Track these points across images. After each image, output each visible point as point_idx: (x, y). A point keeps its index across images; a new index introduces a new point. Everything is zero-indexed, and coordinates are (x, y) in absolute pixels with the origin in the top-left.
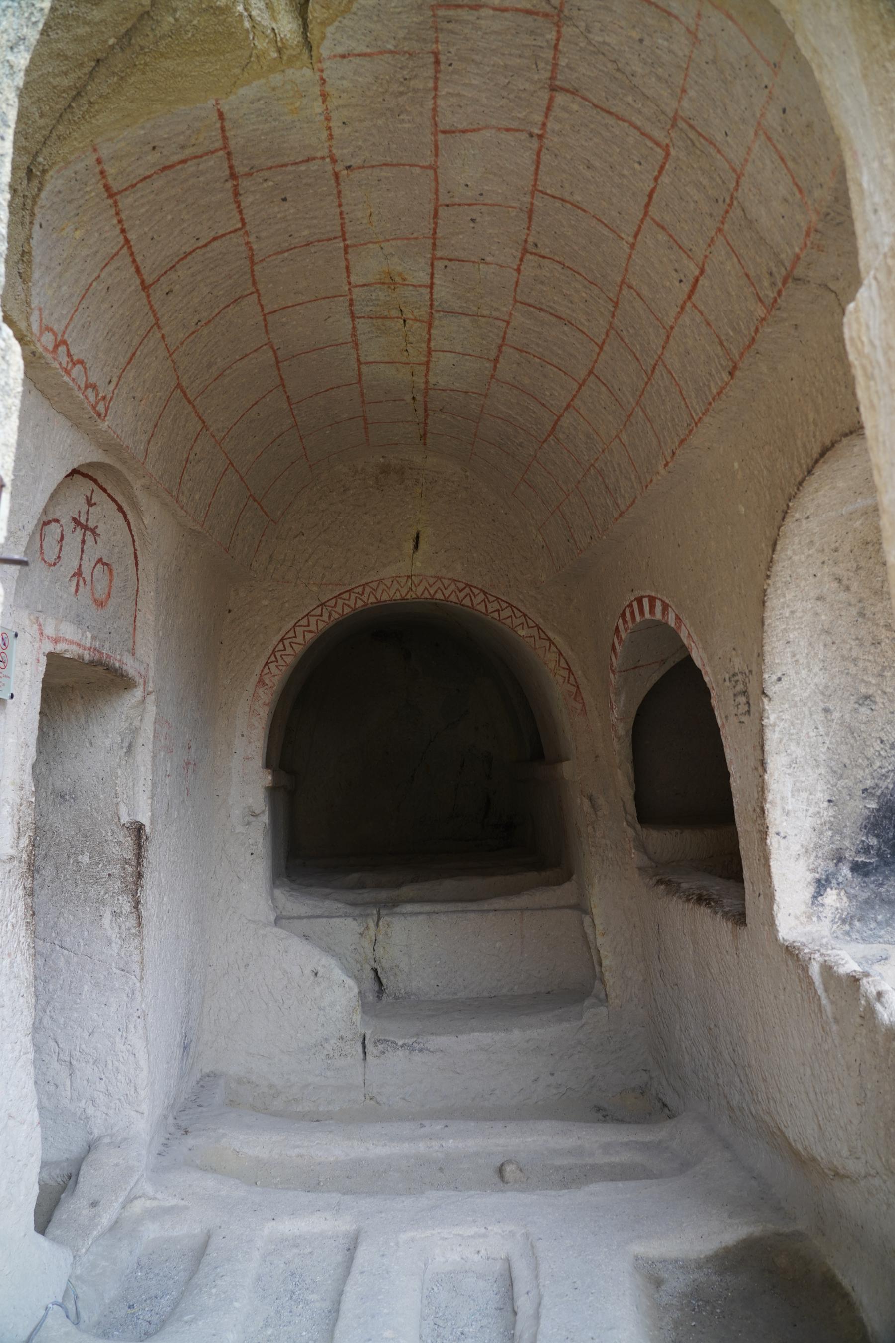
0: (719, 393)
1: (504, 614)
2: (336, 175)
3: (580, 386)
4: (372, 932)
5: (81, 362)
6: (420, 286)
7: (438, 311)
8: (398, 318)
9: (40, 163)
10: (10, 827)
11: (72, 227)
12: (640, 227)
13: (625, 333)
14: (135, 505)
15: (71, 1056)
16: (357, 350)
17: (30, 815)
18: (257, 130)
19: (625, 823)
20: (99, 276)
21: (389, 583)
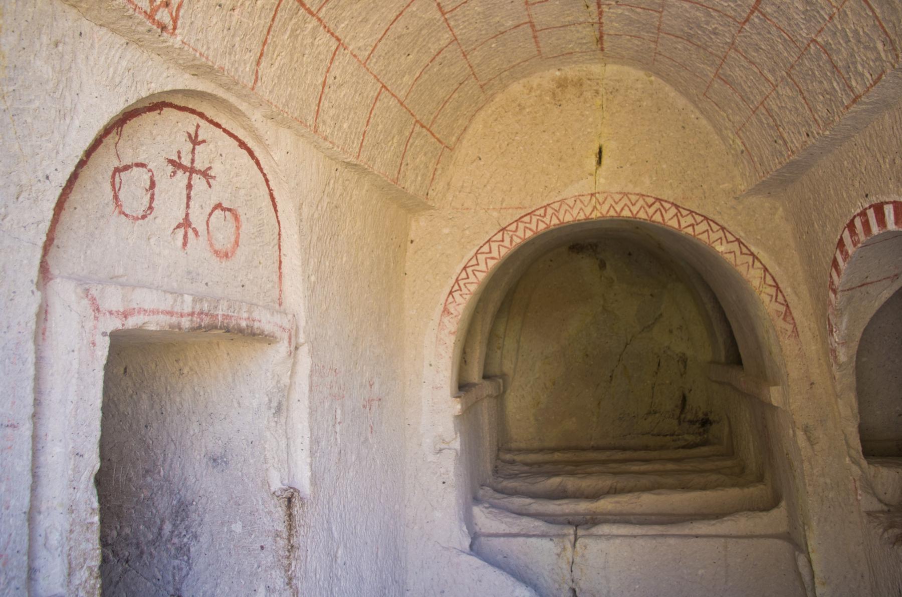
10: (58, 560)
14: (259, 139)
19: (847, 459)
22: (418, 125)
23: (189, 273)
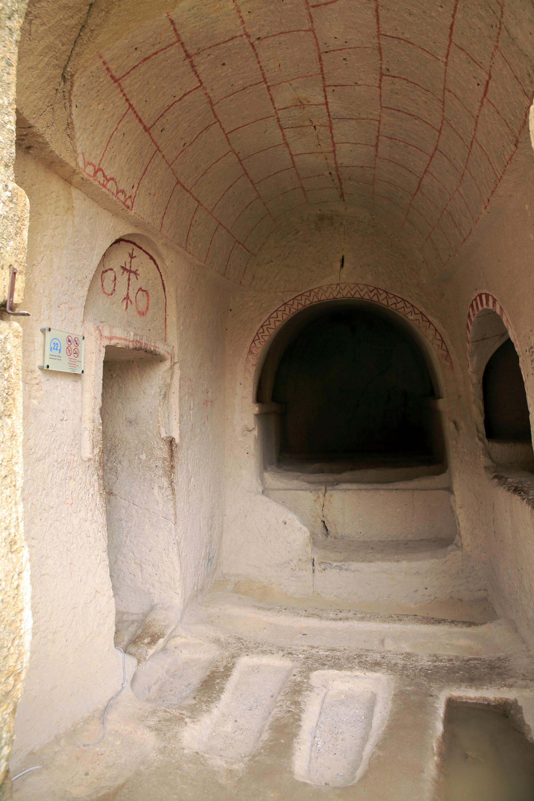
0: (510, 159)
1: (399, 306)
2: (252, 45)
3: (431, 158)
4: (321, 500)
5: (112, 179)
6: (319, 104)
7: (334, 119)
8: (310, 126)
9: (69, 72)
10: (88, 443)
11: (96, 103)
12: (448, 50)
13: (452, 122)
14: (159, 255)
15: (141, 561)
16: (289, 148)
17: (99, 436)
18: (196, 26)
19: (477, 438)
20: (117, 128)
21: (325, 289)
22: (237, 243)
23: (128, 322)
